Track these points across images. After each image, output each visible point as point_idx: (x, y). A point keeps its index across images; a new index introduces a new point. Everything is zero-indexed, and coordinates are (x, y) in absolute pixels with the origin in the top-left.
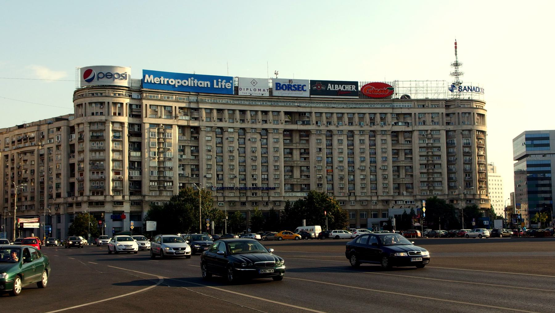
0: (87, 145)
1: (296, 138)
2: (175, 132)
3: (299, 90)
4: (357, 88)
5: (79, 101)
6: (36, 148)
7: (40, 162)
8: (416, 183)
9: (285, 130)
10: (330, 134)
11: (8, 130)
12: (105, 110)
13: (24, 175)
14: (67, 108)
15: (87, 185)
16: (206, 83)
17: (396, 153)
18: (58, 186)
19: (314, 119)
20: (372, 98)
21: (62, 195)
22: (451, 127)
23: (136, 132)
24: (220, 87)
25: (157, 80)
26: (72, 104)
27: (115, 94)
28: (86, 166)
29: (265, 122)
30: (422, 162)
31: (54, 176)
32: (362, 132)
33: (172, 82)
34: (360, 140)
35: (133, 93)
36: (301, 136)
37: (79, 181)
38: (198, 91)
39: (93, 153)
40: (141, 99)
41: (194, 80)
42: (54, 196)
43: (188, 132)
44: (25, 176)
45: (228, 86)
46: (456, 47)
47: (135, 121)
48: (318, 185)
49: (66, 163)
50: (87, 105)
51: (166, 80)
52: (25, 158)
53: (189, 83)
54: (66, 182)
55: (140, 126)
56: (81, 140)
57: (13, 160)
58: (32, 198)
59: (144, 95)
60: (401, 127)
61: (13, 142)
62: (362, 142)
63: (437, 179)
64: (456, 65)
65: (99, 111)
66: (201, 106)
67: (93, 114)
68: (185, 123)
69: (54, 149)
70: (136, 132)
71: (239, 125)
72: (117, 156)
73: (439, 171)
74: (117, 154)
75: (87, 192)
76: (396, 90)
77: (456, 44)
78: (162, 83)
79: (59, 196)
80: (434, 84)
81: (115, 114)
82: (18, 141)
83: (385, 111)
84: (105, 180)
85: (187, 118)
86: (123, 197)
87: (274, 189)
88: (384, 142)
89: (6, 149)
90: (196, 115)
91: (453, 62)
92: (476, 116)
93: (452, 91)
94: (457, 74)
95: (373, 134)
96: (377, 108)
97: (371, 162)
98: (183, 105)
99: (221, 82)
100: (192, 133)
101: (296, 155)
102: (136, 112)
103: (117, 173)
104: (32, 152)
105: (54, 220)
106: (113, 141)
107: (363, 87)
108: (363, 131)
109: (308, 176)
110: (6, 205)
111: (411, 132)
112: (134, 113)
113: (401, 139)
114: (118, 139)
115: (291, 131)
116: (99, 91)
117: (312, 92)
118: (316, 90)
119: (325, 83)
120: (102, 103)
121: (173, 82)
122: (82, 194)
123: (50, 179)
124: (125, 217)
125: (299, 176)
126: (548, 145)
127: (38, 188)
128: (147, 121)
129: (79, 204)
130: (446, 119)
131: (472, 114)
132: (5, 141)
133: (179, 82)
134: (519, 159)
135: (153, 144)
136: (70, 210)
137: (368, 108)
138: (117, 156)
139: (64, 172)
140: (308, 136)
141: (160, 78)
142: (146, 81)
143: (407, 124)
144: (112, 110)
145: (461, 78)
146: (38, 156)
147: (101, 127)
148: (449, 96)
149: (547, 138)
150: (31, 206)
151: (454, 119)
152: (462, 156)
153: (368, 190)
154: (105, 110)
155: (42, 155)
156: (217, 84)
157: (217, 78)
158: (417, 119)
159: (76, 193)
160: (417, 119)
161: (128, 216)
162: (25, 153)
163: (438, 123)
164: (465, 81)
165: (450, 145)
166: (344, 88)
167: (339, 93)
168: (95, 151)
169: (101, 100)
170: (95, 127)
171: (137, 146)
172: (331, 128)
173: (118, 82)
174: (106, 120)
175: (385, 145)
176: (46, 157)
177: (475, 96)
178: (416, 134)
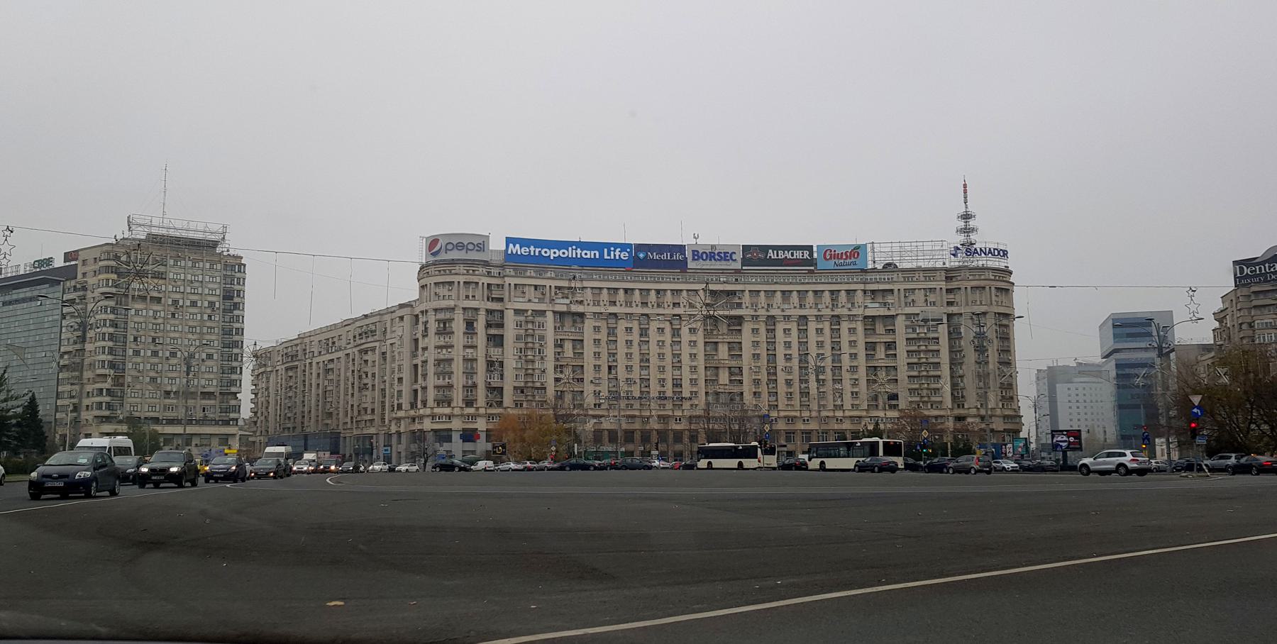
4: (811, 254)
5: (423, 282)
6: (377, 344)
11: (356, 320)
14: (411, 292)
17: (871, 347)
19: (746, 299)
25: (524, 251)
26: (417, 285)
28: (431, 369)
29: (613, 303)
32: (852, 318)
46: (965, 192)
60: (875, 309)
64: (966, 217)
65: (447, 293)
68: (564, 309)
75: (430, 403)
77: (965, 186)
79: (400, 407)
80: (928, 247)
81: (467, 297)
83: (852, 287)
91: (962, 210)
94: (967, 231)
95: (836, 319)
104: (373, 349)
111: (893, 317)
113: (880, 328)
117: (745, 262)
119: (765, 249)
120: (451, 283)
122: (424, 404)
124: (478, 437)
129: (421, 417)
130: (946, 298)
134: (1107, 357)
139: (406, 375)
145: (973, 237)
147: (448, 316)
148: (953, 263)
151: (959, 297)
154: (454, 294)
156: (609, 254)
157: (608, 245)
161: (483, 436)
164: (980, 240)
167: (785, 262)
169: (448, 279)
170: (441, 316)
172: (772, 312)
175: (853, 338)
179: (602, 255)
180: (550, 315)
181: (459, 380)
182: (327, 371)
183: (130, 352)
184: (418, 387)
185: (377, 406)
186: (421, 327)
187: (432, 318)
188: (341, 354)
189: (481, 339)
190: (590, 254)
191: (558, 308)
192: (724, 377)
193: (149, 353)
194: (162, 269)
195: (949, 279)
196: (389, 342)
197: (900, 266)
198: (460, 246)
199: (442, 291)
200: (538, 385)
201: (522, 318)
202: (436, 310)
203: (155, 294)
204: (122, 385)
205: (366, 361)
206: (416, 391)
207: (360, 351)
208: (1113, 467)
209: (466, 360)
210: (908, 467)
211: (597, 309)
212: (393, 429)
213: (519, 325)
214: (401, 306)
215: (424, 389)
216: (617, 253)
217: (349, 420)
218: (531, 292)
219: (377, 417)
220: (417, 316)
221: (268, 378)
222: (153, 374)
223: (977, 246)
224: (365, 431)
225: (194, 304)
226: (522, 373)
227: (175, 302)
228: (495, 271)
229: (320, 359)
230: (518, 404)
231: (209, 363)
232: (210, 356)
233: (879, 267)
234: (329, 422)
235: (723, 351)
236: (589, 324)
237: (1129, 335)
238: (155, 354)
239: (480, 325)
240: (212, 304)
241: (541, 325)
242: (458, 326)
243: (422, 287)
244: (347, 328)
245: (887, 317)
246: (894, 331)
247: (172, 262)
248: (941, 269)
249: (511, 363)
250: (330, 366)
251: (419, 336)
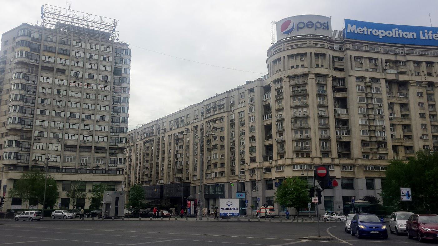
6: (226, 114)
7: (230, 127)
12: (306, 63)
13: (213, 143)
15: (289, 148)
16: (411, 34)
18: (252, 149)
21: (257, 160)
24: (427, 38)
28: (288, 126)
31: (247, 140)
33: (376, 32)
35: (334, 44)
37: (278, 142)
39: (295, 110)
41: (398, 31)
42: (248, 161)
44: (215, 143)
49: (260, 124)
51: (369, 30)
52: (215, 125)
54: (261, 145)
56: (279, 99)
57: (202, 129)
58: (223, 165)
61: (202, 113)
65: (299, 63)
67: (293, 67)
68: (393, 77)
78: (366, 33)
79: (253, 160)
82: (208, 110)
89: (195, 121)
99: (428, 33)
104: (221, 119)
105: (248, 187)
110: (195, 174)
112: (336, 67)
123: (242, 144)
127: (228, 153)
129: (280, 168)
132: (194, 113)
133: (382, 33)
136: (267, 176)
139: (259, 133)
141: (363, 28)
146: (228, 122)
150: (222, 173)
154: (306, 63)
155: (232, 120)
156: (424, 36)
157: (423, 29)
159: (275, 156)
168: (297, 107)
169: (302, 51)
170: (296, 81)
174: (309, 72)
176: (236, 122)
179: (418, 35)
180: (383, 82)
181: (315, 134)
182: (177, 140)
183: (38, 112)
185: (227, 161)
190: (410, 35)
191: (390, 77)
193: (53, 113)
194: (67, 48)
198: (310, 25)
199: (295, 62)
200: (380, 140)
201: (363, 84)
203: (61, 67)
204: (30, 139)
207: (209, 122)
209: (320, 117)
211: (419, 79)
212: (247, 177)
213: (360, 90)
216: (430, 35)
218: (367, 64)
219: (227, 169)
221: (130, 151)
222: (56, 131)
224: (216, 181)
225: (91, 77)
226: (367, 129)
227: (76, 75)
228: (336, 47)
229: (172, 133)
230: (365, 156)
231: (102, 123)
232: (103, 118)
234: (180, 175)
236: (412, 91)
238: (58, 114)
239: (329, 89)
240: (105, 78)
241: (378, 90)
242: (312, 88)
247: (74, 43)
249: (357, 120)
250: (180, 136)
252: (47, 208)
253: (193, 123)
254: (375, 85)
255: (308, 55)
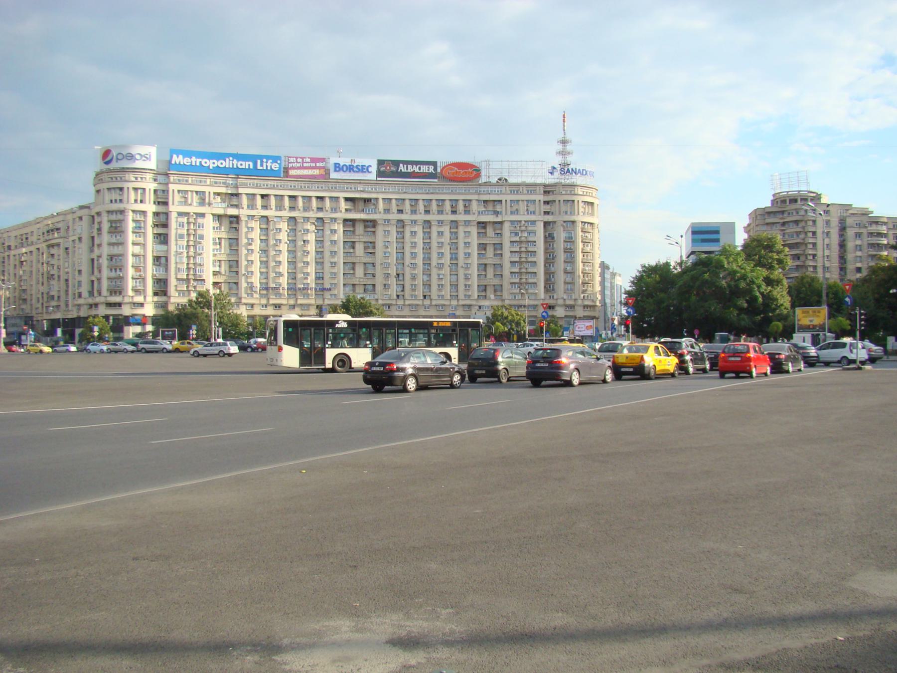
0: (106, 238)
1: (360, 229)
2: (209, 223)
3: (363, 172)
4: (435, 169)
8: (506, 286)
9: (345, 220)
10: (401, 223)
15: (105, 284)
16: (247, 163)
17: (483, 247)
19: (245, 200)
20: (454, 181)
21: (83, 296)
22: (549, 218)
23: (162, 222)
25: (187, 161)
26: (93, 190)
27: (136, 178)
28: (104, 262)
30: (513, 260)
34: (438, 232)
36: (365, 227)
38: (238, 173)
40: (167, 184)
43: (226, 222)
45: (275, 166)
47: (161, 209)
48: (385, 285)
50: (176, 192)
51: (198, 160)
53: (227, 163)
55: (167, 214)
59: (172, 178)
60: (490, 218)
62: (440, 234)
63: (530, 281)
65: (118, 198)
66: (241, 191)
68: (221, 212)
69: (77, 241)
70: (162, 222)
71: (286, 214)
72: (137, 250)
73: (534, 270)
74: (138, 247)
75: (105, 292)
76: (483, 173)
77: (564, 116)
79: (80, 296)
81: (136, 201)
84: (122, 278)
85: (224, 205)
86: (145, 297)
87: (330, 289)
88: (467, 234)
90: (235, 201)
91: (560, 136)
92: (581, 204)
93: (551, 173)
94: (563, 153)
96: (460, 193)
97: (451, 259)
98: (223, 190)
100: (231, 222)
101: (360, 249)
102: (162, 201)
103: (137, 268)
104: (58, 245)
106: (133, 232)
107: (444, 168)
108: (389, 221)
109: (374, 275)
111: (501, 223)
114: (139, 229)
115: (353, 222)
116: (118, 175)
117: (380, 174)
118: (384, 172)
119: (396, 163)
121: (211, 163)
122: (100, 294)
125: (362, 275)
126: (717, 240)
128: (174, 208)
129: (96, 305)
131: (576, 202)
135: (181, 236)
137: (448, 193)
138: (137, 250)
139: (85, 268)
140: (374, 226)
142: (173, 162)
143: (497, 213)
144: (563, 208)
145: (569, 159)
147: (120, 217)
148: (550, 180)
149: (717, 232)
150: (58, 307)
151: (554, 208)
152: (562, 253)
153: (447, 291)
155: (67, 249)
156: (262, 165)
157: (261, 157)
158: (509, 207)
159: (96, 294)
160: (509, 207)
162: (52, 246)
163: (534, 213)
164: (575, 162)
165: (549, 238)
166: (420, 169)
169: (119, 185)
170: (113, 217)
171: (162, 239)
173: (139, 164)
177: (578, 180)
178: (507, 226)
184: (93, 278)
186: (96, 226)
187: (105, 218)
188: (33, 248)
189: (379, 244)
190: (245, 165)
192: (360, 271)
195: (546, 193)
196: (71, 238)
197: (511, 180)
202: (108, 212)
205: (53, 255)
206: (93, 282)
208: (217, 352)
210: (80, 350)
214: (82, 207)
215: (99, 280)
217: (40, 305)
219: (62, 304)
220: (93, 217)
223: (570, 167)
233: (494, 180)
234: (24, 307)
235: (360, 249)
237: (704, 241)
243: (98, 191)
244: (38, 226)
245: (496, 223)
246: (501, 234)
248: (540, 185)
251: (95, 234)
252: (289, 341)
253: (36, 243)
254: (200, 220)
255: (537, 202)
